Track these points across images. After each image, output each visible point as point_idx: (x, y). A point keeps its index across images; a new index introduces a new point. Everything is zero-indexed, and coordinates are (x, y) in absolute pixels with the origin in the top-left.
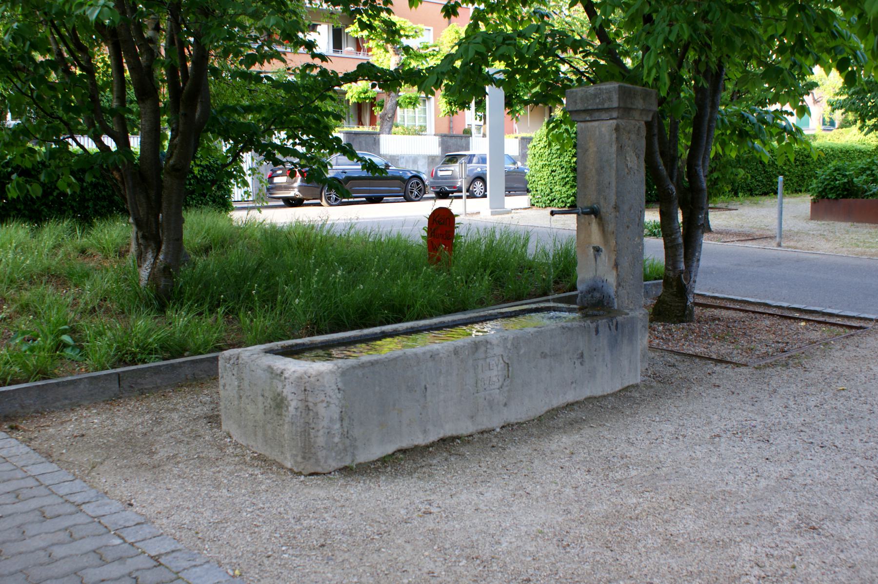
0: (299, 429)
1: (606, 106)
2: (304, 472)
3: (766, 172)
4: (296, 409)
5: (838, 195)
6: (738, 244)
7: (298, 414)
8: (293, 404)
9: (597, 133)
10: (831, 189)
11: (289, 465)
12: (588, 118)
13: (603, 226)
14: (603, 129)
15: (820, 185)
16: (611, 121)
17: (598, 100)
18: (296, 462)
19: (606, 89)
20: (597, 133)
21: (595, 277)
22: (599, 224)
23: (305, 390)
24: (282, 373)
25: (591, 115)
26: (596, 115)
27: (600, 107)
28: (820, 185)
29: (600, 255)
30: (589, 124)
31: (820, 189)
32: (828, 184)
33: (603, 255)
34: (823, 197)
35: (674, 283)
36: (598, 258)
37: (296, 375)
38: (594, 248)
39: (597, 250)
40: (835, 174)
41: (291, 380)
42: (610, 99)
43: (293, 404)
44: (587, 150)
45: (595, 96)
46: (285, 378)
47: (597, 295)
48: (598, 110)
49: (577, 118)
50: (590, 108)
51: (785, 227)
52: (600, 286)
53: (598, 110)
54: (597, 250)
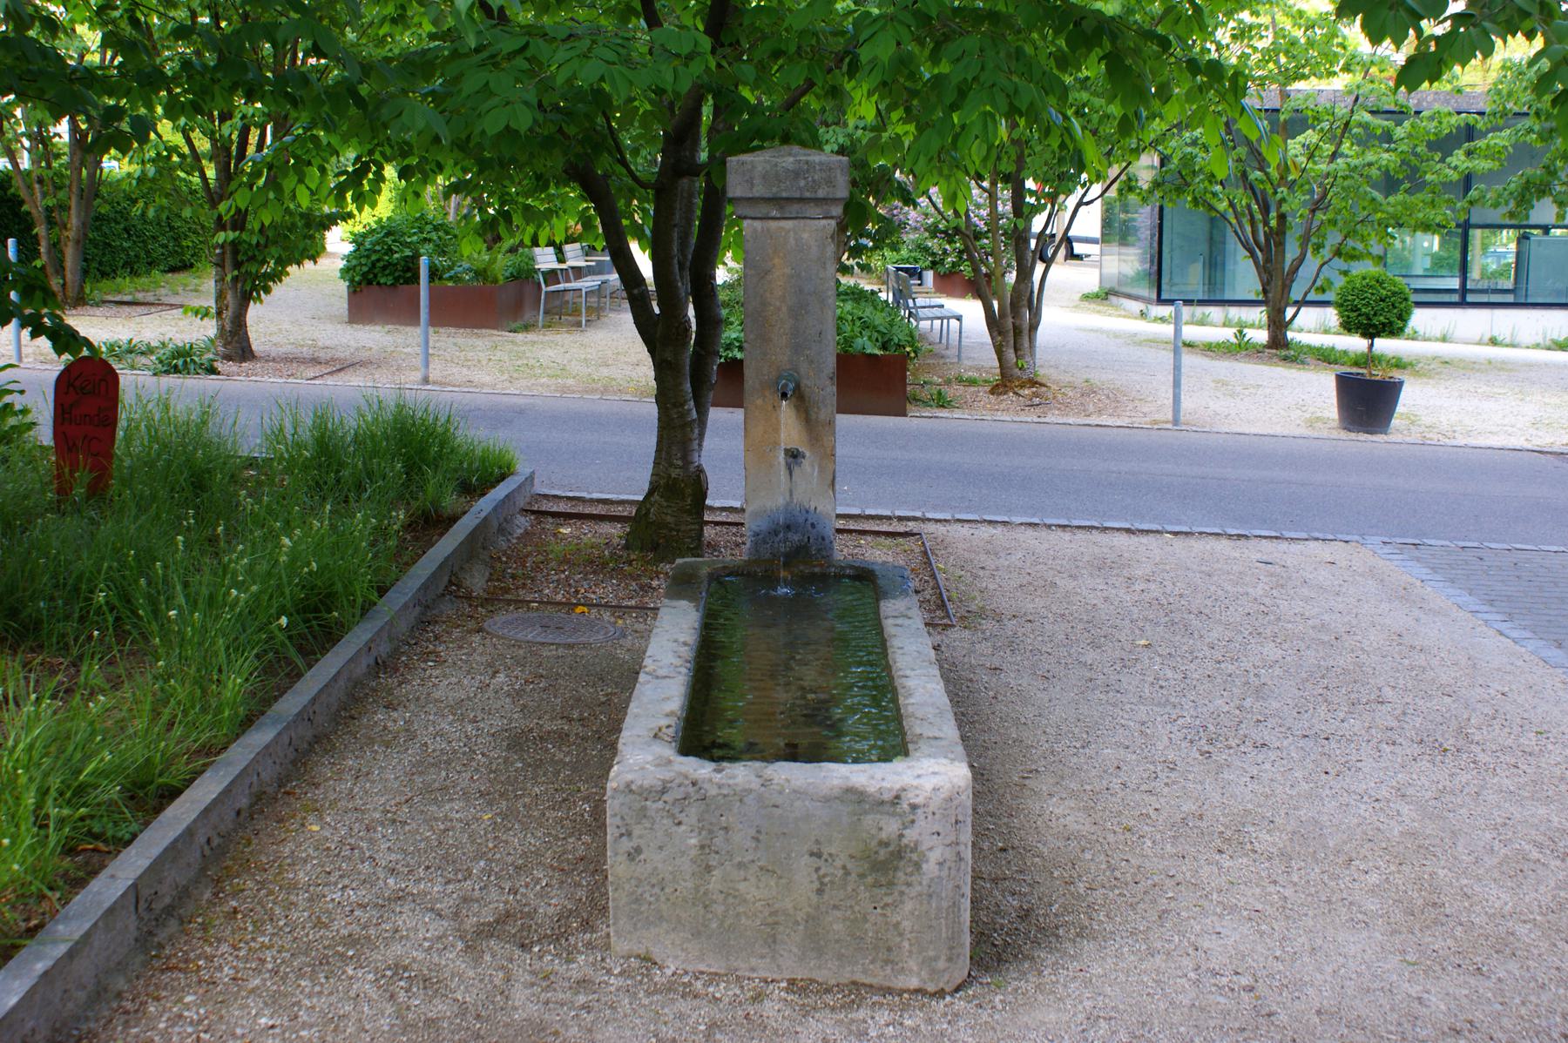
0: (945, 904)
1: (821, 194)
2: (947, 989)
3: (172, 228)
4: (940, 864)
5: (396, 279)
6: (330, 381)
7: (945, 873)
8: (934, 856)
9: (792, 241)
10: (384, 268)
11: (914, 983)
12: (774, 213)
13: (807, 412)
14: (805, 236)
15: (363, 261)
16: (824, 222)
17: (802, 183)
18: (933, 971)
19: (821, 163)
20: (792, 241)
21: (788, 504)
22: (797, 408)
23: (957, 822)
24: (897, 797)
25: (782, 208)
26: (794, 209)
27: (808, 195)
28: (363, 261)
29: (800, 465)
30: (773, 224)
31: (365, 269)
32: (378, 260)
33: (806, 463)
34: (370, 283)
35: (689, 491)
36: (796, 471)
37: (943, 794)
38: (786, 451)
39: (794, 455)
40: (389, 240)
41: (931, 809)
42: (830, 182)
43: (934, 856)
44: (767, 272)
45: (797, 174)
46: (914, 807)
47: (795, 538)
48: (801, 200)
49: (748, 212)
50: (784, 195)
51: (1187, 404)
52: (801, 520)
53: (801, 200)
54: (794, 455)
